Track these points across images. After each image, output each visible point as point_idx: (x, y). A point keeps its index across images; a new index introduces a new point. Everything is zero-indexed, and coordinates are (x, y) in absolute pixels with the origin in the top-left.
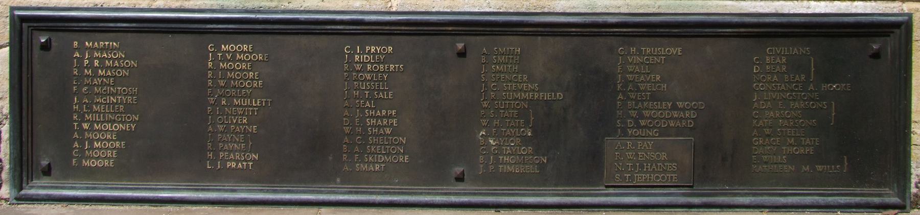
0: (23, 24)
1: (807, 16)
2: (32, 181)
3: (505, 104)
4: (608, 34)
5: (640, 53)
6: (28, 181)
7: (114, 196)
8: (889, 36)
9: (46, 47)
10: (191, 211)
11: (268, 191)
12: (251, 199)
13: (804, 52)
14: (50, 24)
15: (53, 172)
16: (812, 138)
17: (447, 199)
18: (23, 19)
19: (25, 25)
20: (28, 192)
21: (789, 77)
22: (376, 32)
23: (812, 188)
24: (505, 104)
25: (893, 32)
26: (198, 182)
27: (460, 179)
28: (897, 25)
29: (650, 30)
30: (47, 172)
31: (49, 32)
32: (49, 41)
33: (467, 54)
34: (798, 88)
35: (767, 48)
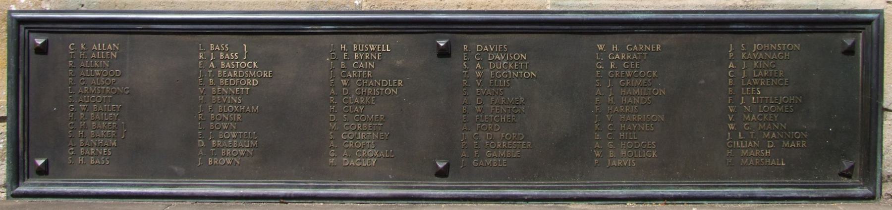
0: (21, 26)
1: (826, 13)
2: (24, 180)
3: (760, 99)
4: (658, 31)
5: (622, 49)
6: (24, 177)
7: (84, 192)
8: (861, 32)
9: (42, 50)
10: (490, 207)
11: (371, 187)
12: (337, 194)
13: (775, 48)
14: (834, 27)
15: (50, 171)
16: (240, 132)
17: (381, 192)
18: (21, 21)
19: (22, 27)
20: (22, 189)
21: (222, 73)
22: (257, 31)
23: (466, 182)
24: (760, 99)
25: (864, 29)
26: (241, 179)
27: (847, 175)
28: (869, 22)
29: (755, 27)
30: (43, 172)
31: (48, 34)
32: (46, 44)
33: (452, 55)
34: (784, 84)
35: (69, 46)
